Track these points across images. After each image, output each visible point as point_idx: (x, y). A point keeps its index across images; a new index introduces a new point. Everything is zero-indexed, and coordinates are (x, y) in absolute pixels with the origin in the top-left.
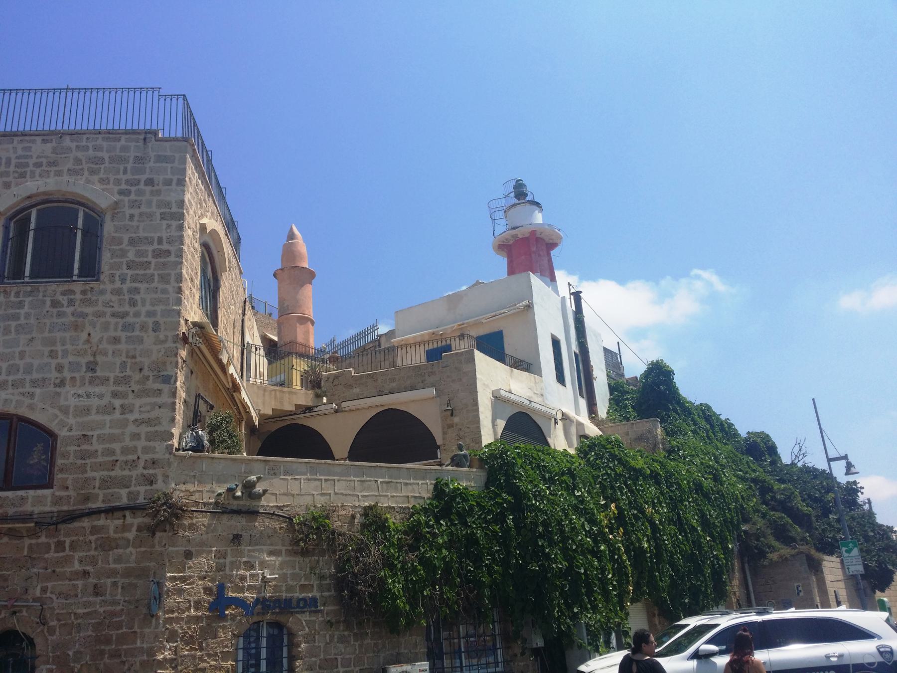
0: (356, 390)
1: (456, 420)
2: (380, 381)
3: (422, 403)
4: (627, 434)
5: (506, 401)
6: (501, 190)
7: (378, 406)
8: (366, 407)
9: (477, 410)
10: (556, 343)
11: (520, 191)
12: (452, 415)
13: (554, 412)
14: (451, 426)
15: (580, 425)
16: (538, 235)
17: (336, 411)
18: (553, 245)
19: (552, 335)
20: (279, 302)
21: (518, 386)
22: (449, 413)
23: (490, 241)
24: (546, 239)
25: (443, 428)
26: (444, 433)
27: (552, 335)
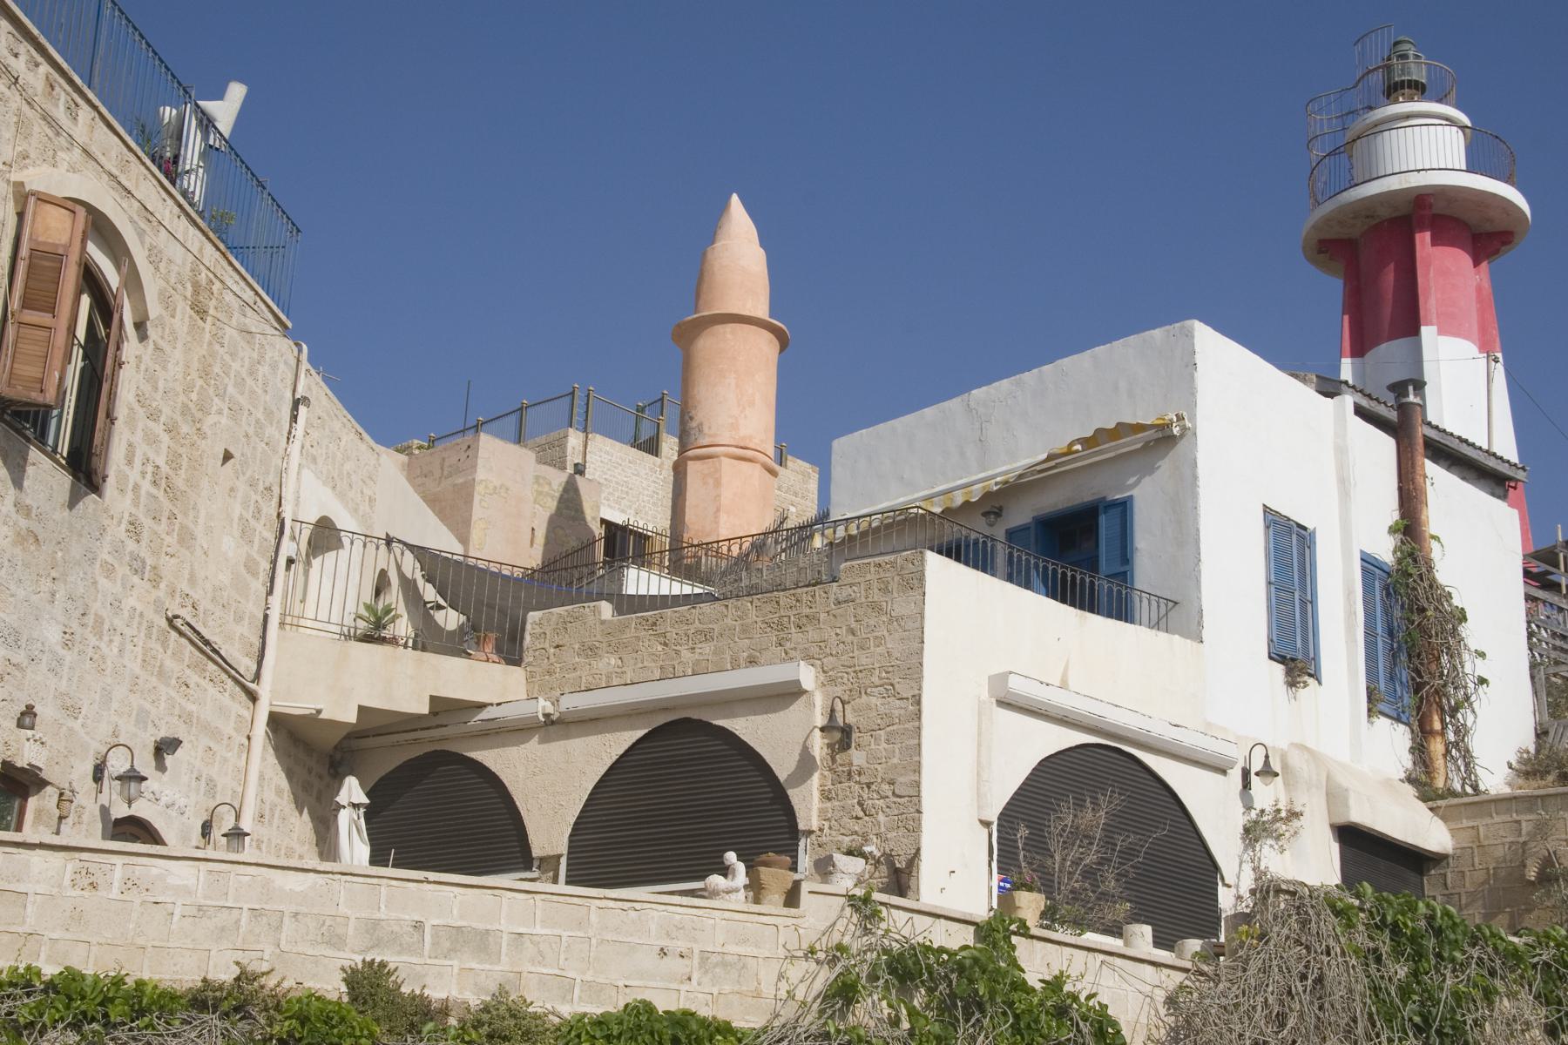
19: (1267, 510)
27: (1267, 510)
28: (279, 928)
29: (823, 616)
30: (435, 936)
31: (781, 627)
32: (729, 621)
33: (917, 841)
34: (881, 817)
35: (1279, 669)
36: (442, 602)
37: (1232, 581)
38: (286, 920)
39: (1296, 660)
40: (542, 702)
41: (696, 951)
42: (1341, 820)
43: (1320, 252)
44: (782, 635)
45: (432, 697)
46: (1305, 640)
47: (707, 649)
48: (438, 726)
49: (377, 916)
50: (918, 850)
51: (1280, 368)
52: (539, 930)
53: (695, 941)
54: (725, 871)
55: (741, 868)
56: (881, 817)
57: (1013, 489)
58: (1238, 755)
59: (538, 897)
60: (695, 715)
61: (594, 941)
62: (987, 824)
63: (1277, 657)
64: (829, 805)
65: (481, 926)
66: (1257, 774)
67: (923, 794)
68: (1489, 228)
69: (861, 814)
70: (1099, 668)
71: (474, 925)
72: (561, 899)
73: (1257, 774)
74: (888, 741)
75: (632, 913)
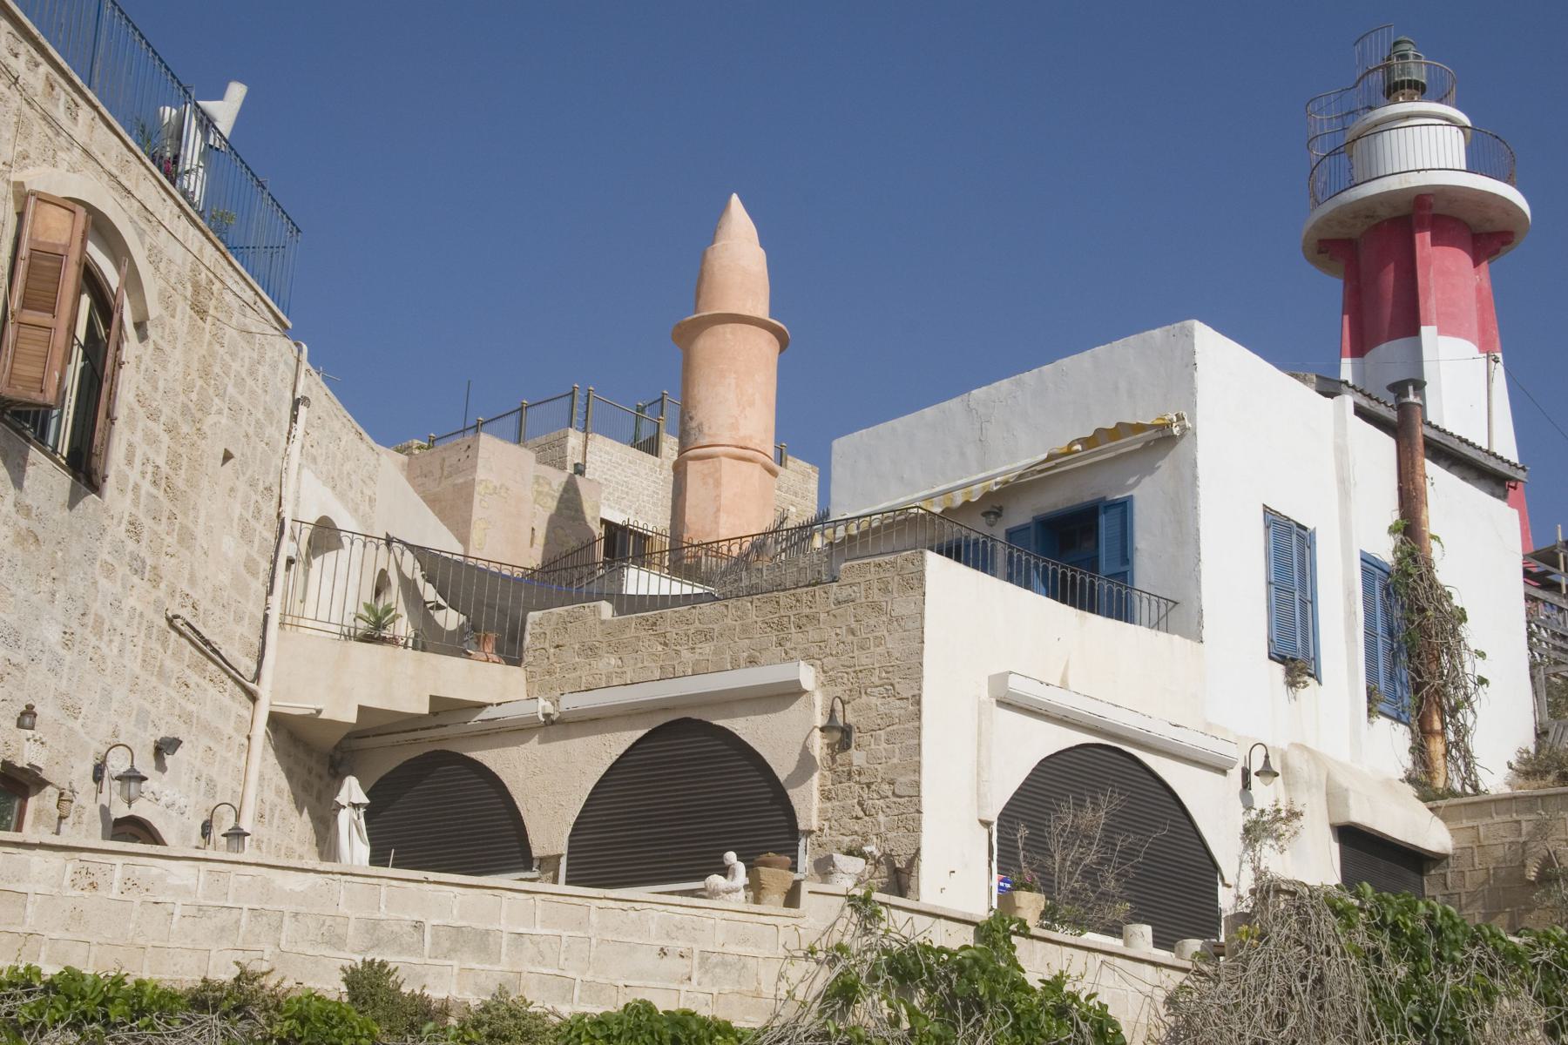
10: (1289, 546)
19: (1267, 510)
27: (1267, 510)
28: (279, 928)
29: (823, 616)
30: (435, 936)
31: (781, 627)
32: (729, 621)
33: (917, 841)
34: (881, 818)
35: (1279, 669)
37: (1232, 581)
38: (286, 919)
39: (1296, 660)
40: (542, 702)
41: (696, 952)
42: (1341, 820)
46: (1305, 640)
47: (707, 648)
49: (378, 916)
50: (918, 850)
52: (539, 930)
53: (695, 941)
54: (725, 871)
55: (741, 868)
56: (881, 818)
57: (1013, 490)
59: (538, 897)
60: (695, 715)
61: (594, 941)
62: (987, 824)
63: (1277, 657)
64: (829, 805)
65: (481, 926)
66: (1257, 774)
67: (923, 794)
69: (861, 814)
70: (1099, 668)
72: (561, 899)
73: (1257, 774)
74: (888, 741)
75: (632, 914)
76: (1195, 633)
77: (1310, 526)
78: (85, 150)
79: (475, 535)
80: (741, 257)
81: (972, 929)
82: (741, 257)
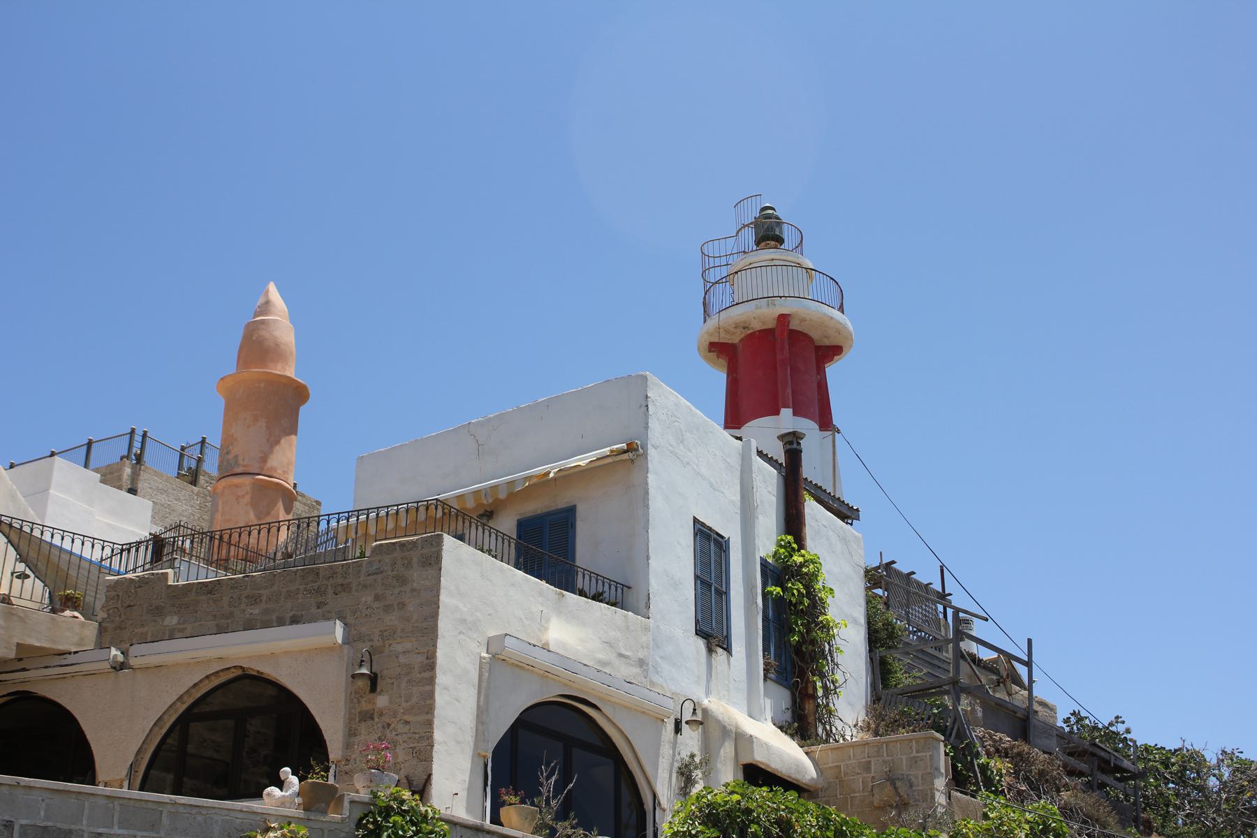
0: (172, 621)
1: (382, 701)
2: (226, 600)
3: (304, 656)
4: (867, 766)
5: (520, 667)
6: (727, 226)
7: (565, 685)
8: (193, 659)
9: (432, 681)
10: (709, 544)
11: (768, 232)
12: (373, 688)
13: (670, 704)
14: (367, 716)
15: (742, 740)
16: (794, 325)
17: (119, 667)
18: (835, 351)
19: (696, 520)
20: (224, 440)
21: (568, 635)
22: (363, 684)
23: (698, 331)
24: (814, 334)
25: (350, 720)
26: (351, 733)
27: (696, 520)
31: (320, 591)
35: (701, 643)
36: (28, 572)
37: (671, 570)
39: (713, 634)
40: (114, 651)
42: (747, 760)
43: (710, 351)
44: (321, 599)
45: (18, 645)
46: (720, 623)
48: (24, 670)
50: (430, 775)
51: (83, 732)
54: (280, 784)
55: (295, 780)
57: (515, 495)
58: (672, 707)
63: (699, 633)
65: (65, 827)
66: (687, 723)
68: (827, 342)
70: (568, 635)
71: (59, 825)
73: (687, 723)
76: (643, 609)
77: (726, 535)
78: (712, 485)
79: (51, 508)
80: (273, 290)
81: (973, 633)
82: (273, 290)
